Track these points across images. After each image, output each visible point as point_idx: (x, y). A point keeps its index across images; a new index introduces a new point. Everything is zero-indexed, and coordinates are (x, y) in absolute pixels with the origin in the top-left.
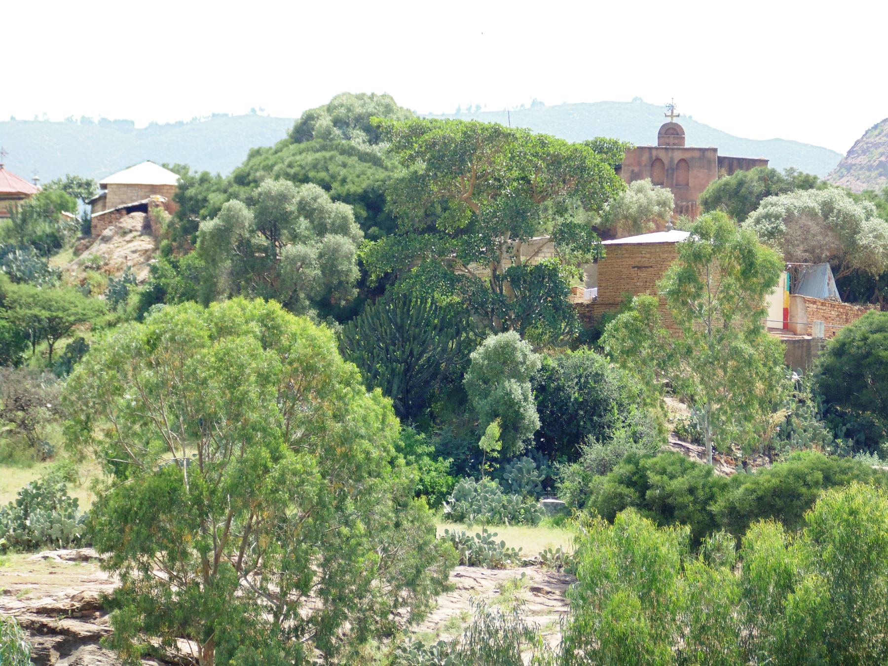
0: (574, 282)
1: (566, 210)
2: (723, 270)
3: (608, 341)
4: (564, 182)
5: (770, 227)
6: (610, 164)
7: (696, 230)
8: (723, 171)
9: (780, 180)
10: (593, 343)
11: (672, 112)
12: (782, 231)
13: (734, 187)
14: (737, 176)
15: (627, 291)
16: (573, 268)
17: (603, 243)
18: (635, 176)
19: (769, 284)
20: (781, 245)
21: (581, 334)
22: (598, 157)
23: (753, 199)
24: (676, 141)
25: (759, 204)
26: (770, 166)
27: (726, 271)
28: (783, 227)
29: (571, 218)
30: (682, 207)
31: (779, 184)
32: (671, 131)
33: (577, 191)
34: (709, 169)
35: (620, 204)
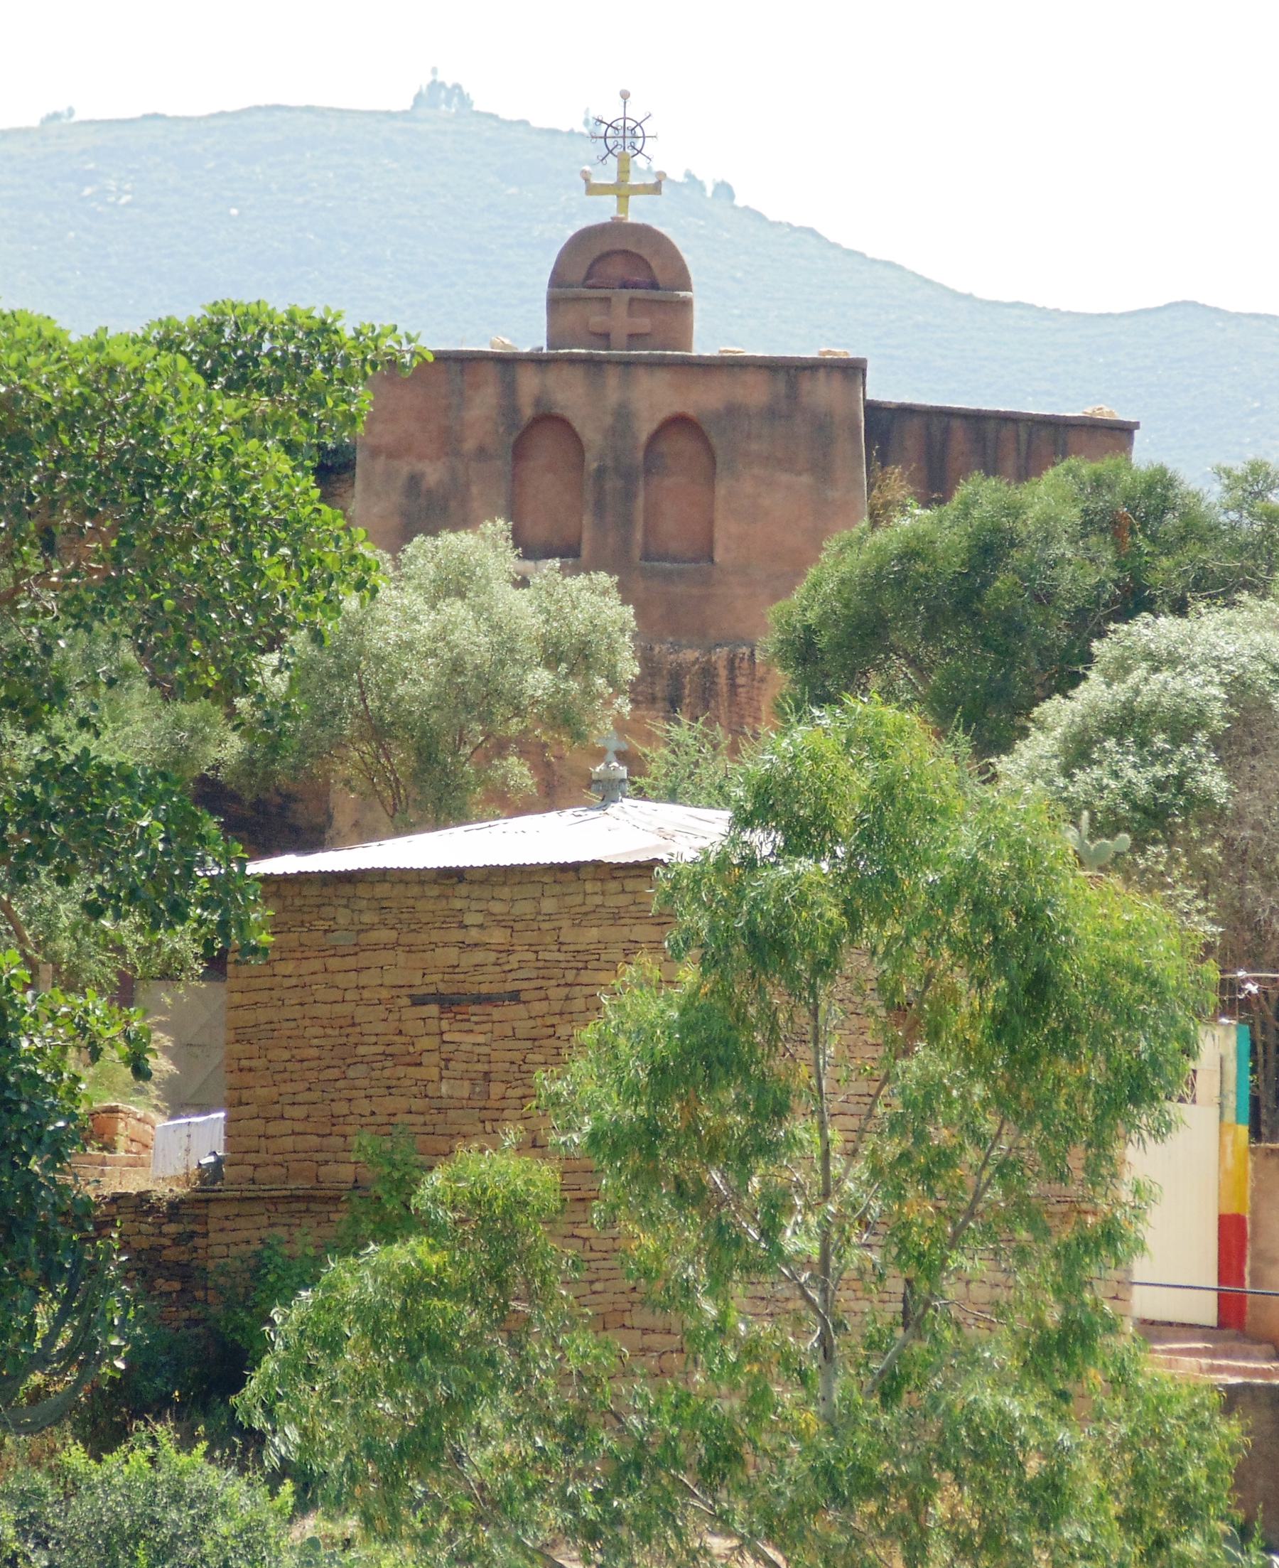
0: (99, 1087)
1: (59, 693)
2: (898, 1010)
3: (293, 1405)
4: (48, 544)
5: (1142, 782)
6: (290, 448)
7: (765, 805)
8: (897, 483)
9: (1196, 530)
10: (206, 1411)
11: (624, 171)
12: (1208, 801)
13: (956, 565)
14: (967, 507)
15: (386, 1127)
16: (97, 1005)
17: (258, 867)
18: (427, 511)
19: (1138, 1089)
20: (1205, 878)
21: (141, 1361)
22: (228, 406)
23: (1059, 634)
24: (643, 323)
25: (1088, 658)
26: (1145, 454)
27: (911, 1019)
28: (1213, 781)
29: (84, 738)
30: (676, 676)
31: (1193, 548)
32: (617, 269)
33: (113, 590)
34: (822, 470)
35: (344, 663)
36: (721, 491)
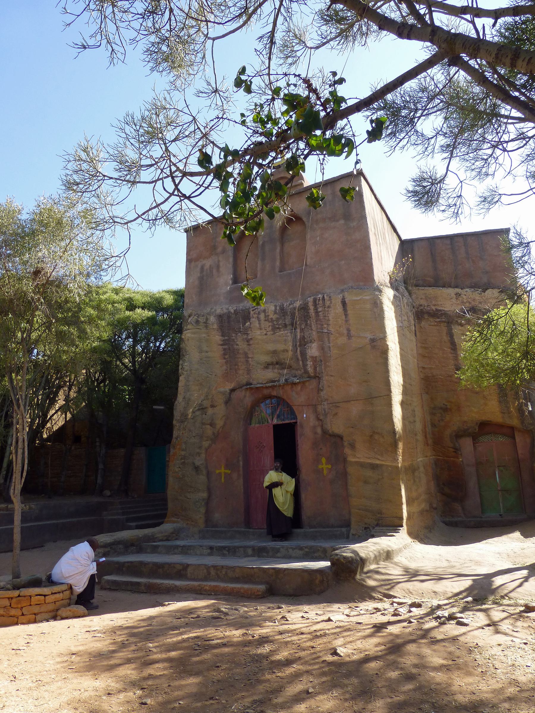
36: (308, 236)
